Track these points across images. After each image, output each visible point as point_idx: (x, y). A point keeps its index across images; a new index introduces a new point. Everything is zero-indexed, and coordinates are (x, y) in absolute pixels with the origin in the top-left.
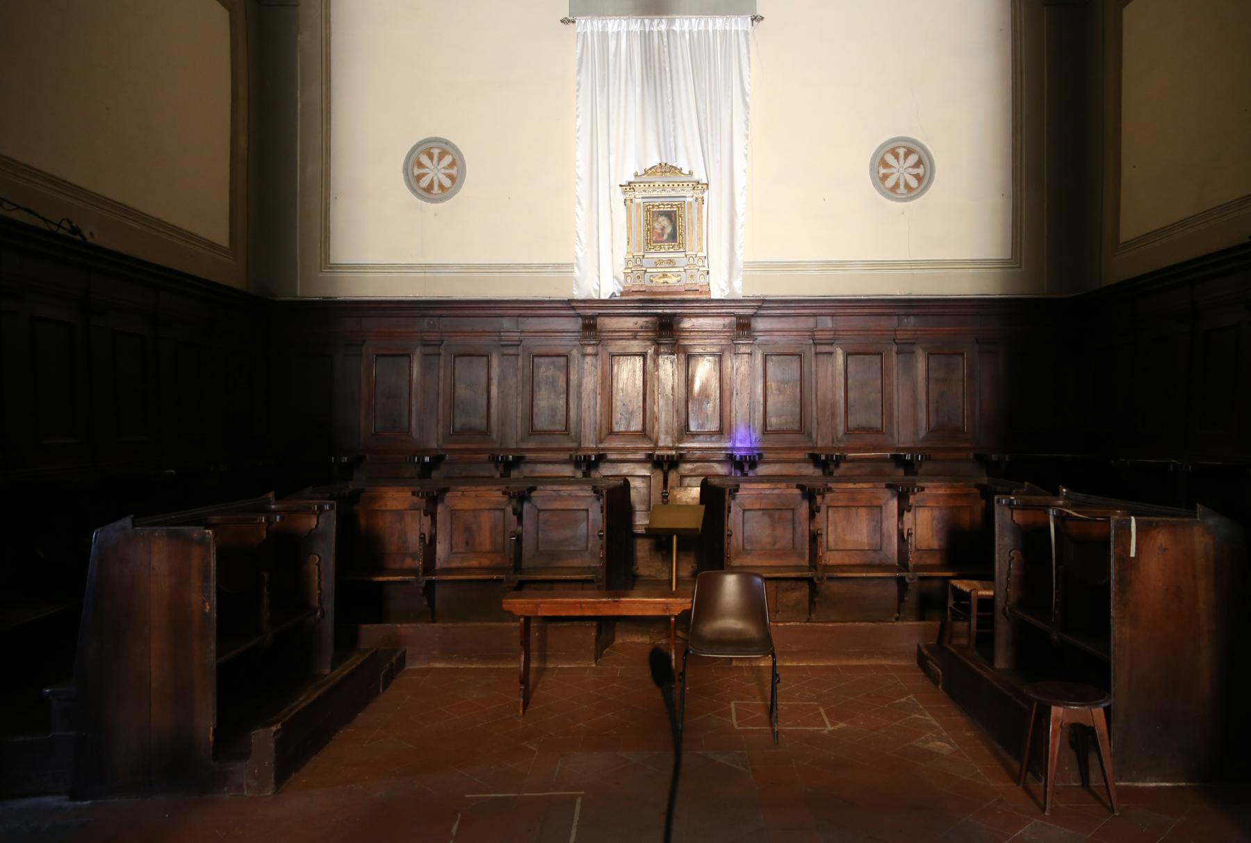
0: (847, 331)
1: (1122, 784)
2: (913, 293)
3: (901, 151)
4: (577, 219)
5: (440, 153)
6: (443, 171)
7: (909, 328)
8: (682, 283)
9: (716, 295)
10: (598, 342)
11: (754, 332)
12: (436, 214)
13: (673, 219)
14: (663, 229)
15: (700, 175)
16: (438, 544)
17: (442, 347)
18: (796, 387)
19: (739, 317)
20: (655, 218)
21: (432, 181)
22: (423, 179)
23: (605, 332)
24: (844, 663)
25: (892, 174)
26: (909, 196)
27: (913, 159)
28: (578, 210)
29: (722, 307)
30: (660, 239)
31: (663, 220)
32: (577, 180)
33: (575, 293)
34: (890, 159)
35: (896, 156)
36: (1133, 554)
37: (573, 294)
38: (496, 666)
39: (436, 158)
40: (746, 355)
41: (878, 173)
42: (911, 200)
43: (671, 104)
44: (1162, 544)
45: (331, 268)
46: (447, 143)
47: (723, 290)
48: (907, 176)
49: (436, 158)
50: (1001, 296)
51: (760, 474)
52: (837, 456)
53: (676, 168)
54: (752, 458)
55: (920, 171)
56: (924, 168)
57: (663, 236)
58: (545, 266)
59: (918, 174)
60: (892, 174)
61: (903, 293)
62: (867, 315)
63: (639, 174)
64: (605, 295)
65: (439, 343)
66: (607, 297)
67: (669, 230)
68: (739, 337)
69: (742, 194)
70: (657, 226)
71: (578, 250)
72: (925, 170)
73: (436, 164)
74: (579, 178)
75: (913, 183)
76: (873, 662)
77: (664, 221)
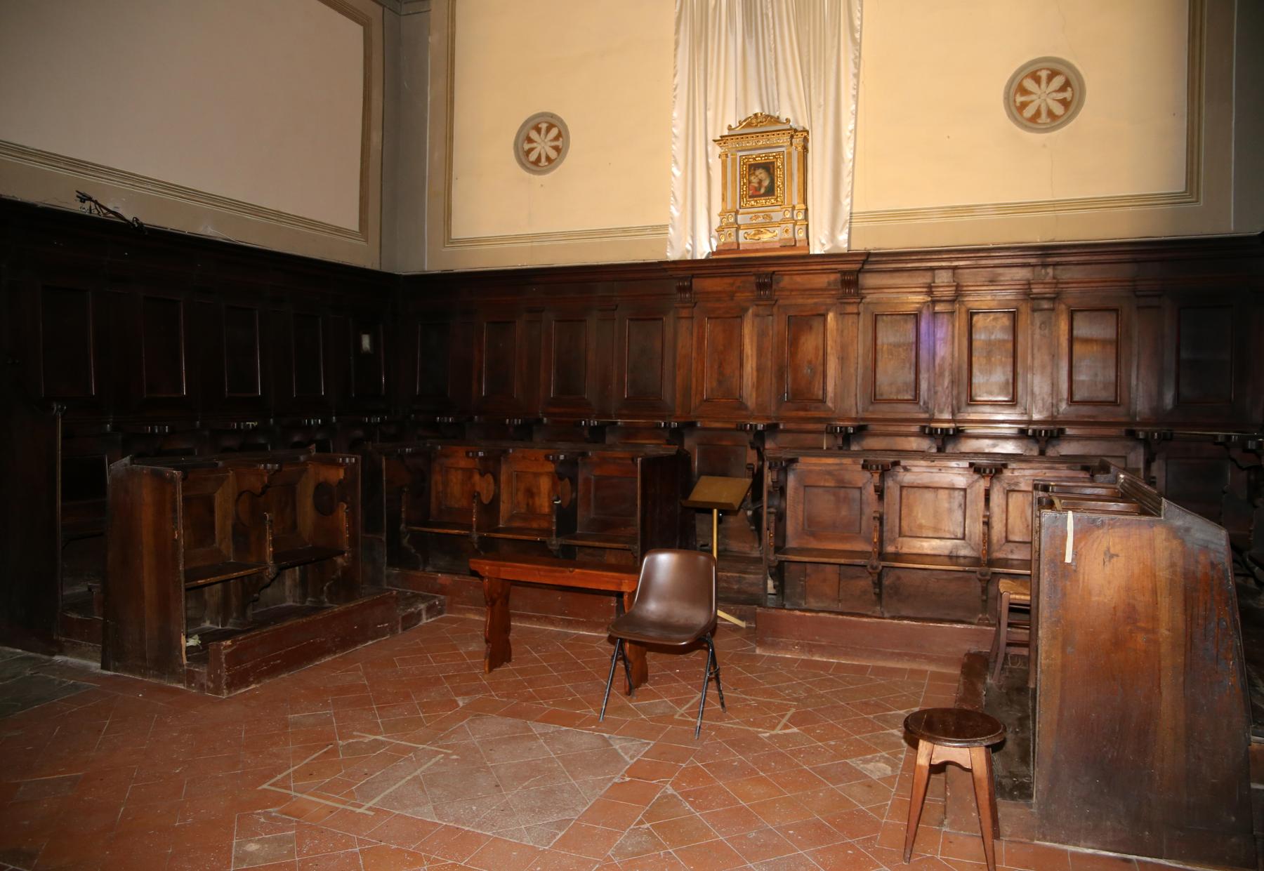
0: (1105, 282)
1: (1047, 844)
2: (1056, 240)
3: (1044, 74)
4: (673, 179)
5: (547, 127)
6: (550, 144)
7: (1047, 281)
8: (776, 239)
9: (816, 249)
10: (859, 300)
11: (862, 289)
12: (542, 186)
13: (771, 171)
14: (760, 182)
15: (803, 123)
16: (501, 503)
17: (861, 305)
18: (911, 350)
19: (844, 273)
20: (752, 172)
21: (540, 155)
22: (533, 153)
23: (866, 289)
24: (881, 663)
25: (1032, 101)
26: (1053, 125)
27: (1058, 82)
28: (674, 170)
29: (828, 263)
30: (758, 193)
31: (761, 173)
32: (674, 139)
33: (668, 254)
34: (1029, 84)
35: (1037, 80)
36: (1068, 559)
37: (667, 255)
38: (576, 632)
39: (543, 131)
40: (946, 316)
41: (1015, 101)
42: (1054, 130)
43: (773, 51)
44: (1108, 549)
45: (452, 243)
46: (552, 116)
47: (823, 245)
48: (1050, 102)
49: (543, 131)
50: (1166, 238)
51: (1063, 453)
52: (751, 425)
53: (772, 117)
54: (843, 429)
55: (1067, 95)
56: (1073, 90)
57: (760, 189)
58: (644, 229)
59: (1065, 99)
60: (1032, 101)
61: (1044, 240)
62: (1124, 262)
63: (733, 127)
64: (701, 255)
65: (614, 307)
66: (703, 257)
67: (766, 183)
68: (844, 296)
69: (849, 138)
70: (754, 180)
71: (673, 209)
72: (1073, 94)
73: (543, 138)
74: (676, 137)
75: (1058, 109)
76: (915, 666)
77: (761, 174)
